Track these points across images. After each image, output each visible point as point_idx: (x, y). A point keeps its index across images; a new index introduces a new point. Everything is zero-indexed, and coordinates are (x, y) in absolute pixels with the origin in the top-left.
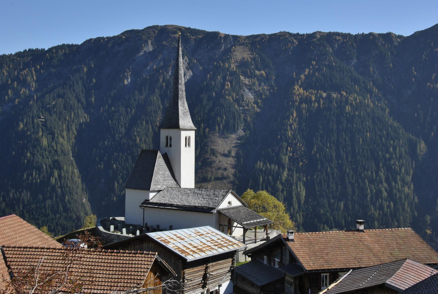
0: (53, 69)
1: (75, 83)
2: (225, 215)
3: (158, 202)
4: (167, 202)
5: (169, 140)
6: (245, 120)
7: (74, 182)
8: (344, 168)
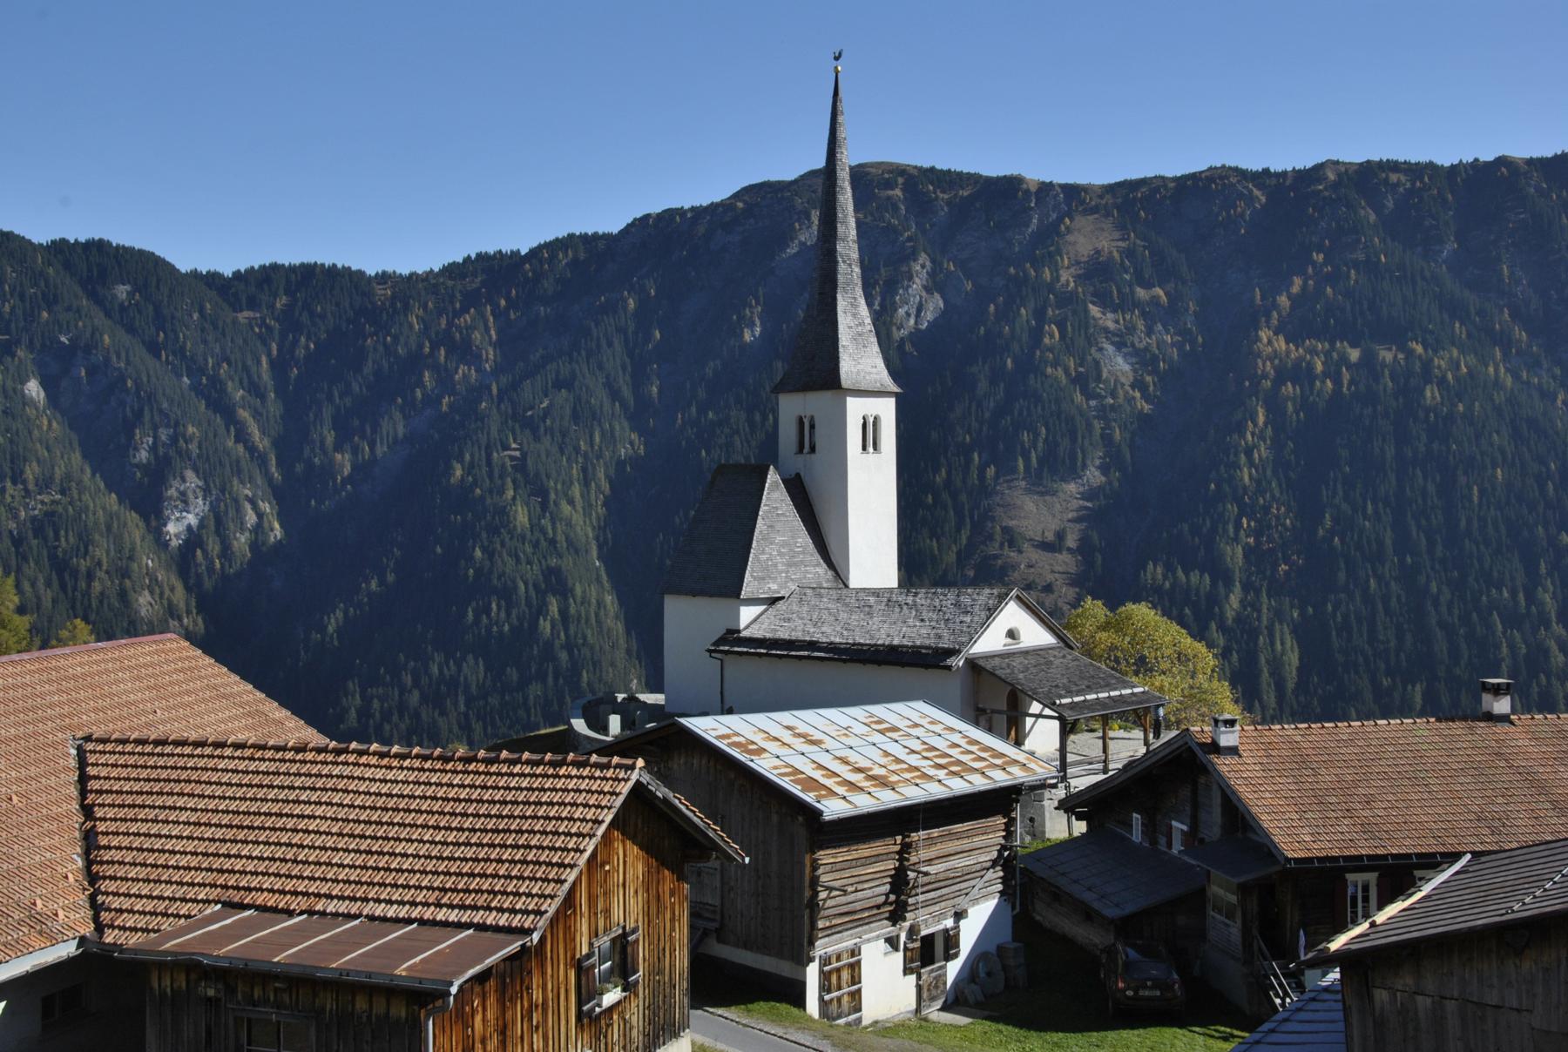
0: (542, 308)
1: (604, 342)
2: (992, 674)
3: (768, 635)
4: (798, 635)
5: (806, 431)
6: (1107, 439)
7: (605, 631)
8: (1422, 579)
